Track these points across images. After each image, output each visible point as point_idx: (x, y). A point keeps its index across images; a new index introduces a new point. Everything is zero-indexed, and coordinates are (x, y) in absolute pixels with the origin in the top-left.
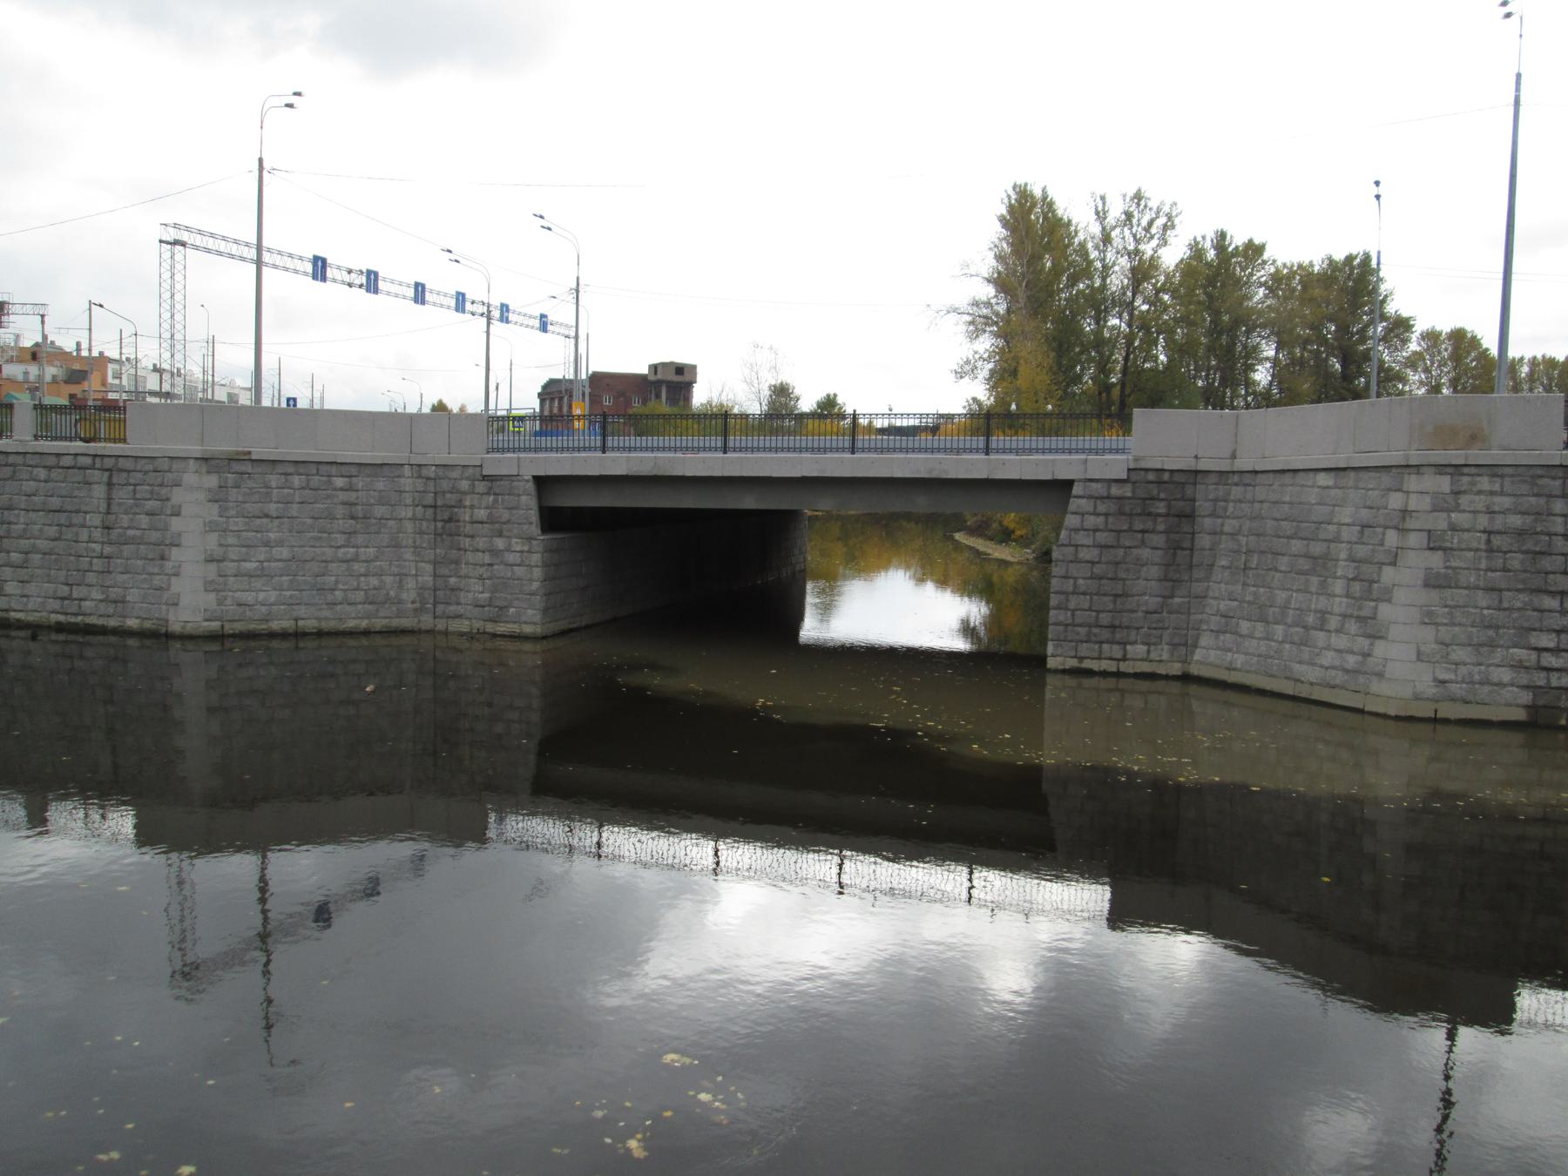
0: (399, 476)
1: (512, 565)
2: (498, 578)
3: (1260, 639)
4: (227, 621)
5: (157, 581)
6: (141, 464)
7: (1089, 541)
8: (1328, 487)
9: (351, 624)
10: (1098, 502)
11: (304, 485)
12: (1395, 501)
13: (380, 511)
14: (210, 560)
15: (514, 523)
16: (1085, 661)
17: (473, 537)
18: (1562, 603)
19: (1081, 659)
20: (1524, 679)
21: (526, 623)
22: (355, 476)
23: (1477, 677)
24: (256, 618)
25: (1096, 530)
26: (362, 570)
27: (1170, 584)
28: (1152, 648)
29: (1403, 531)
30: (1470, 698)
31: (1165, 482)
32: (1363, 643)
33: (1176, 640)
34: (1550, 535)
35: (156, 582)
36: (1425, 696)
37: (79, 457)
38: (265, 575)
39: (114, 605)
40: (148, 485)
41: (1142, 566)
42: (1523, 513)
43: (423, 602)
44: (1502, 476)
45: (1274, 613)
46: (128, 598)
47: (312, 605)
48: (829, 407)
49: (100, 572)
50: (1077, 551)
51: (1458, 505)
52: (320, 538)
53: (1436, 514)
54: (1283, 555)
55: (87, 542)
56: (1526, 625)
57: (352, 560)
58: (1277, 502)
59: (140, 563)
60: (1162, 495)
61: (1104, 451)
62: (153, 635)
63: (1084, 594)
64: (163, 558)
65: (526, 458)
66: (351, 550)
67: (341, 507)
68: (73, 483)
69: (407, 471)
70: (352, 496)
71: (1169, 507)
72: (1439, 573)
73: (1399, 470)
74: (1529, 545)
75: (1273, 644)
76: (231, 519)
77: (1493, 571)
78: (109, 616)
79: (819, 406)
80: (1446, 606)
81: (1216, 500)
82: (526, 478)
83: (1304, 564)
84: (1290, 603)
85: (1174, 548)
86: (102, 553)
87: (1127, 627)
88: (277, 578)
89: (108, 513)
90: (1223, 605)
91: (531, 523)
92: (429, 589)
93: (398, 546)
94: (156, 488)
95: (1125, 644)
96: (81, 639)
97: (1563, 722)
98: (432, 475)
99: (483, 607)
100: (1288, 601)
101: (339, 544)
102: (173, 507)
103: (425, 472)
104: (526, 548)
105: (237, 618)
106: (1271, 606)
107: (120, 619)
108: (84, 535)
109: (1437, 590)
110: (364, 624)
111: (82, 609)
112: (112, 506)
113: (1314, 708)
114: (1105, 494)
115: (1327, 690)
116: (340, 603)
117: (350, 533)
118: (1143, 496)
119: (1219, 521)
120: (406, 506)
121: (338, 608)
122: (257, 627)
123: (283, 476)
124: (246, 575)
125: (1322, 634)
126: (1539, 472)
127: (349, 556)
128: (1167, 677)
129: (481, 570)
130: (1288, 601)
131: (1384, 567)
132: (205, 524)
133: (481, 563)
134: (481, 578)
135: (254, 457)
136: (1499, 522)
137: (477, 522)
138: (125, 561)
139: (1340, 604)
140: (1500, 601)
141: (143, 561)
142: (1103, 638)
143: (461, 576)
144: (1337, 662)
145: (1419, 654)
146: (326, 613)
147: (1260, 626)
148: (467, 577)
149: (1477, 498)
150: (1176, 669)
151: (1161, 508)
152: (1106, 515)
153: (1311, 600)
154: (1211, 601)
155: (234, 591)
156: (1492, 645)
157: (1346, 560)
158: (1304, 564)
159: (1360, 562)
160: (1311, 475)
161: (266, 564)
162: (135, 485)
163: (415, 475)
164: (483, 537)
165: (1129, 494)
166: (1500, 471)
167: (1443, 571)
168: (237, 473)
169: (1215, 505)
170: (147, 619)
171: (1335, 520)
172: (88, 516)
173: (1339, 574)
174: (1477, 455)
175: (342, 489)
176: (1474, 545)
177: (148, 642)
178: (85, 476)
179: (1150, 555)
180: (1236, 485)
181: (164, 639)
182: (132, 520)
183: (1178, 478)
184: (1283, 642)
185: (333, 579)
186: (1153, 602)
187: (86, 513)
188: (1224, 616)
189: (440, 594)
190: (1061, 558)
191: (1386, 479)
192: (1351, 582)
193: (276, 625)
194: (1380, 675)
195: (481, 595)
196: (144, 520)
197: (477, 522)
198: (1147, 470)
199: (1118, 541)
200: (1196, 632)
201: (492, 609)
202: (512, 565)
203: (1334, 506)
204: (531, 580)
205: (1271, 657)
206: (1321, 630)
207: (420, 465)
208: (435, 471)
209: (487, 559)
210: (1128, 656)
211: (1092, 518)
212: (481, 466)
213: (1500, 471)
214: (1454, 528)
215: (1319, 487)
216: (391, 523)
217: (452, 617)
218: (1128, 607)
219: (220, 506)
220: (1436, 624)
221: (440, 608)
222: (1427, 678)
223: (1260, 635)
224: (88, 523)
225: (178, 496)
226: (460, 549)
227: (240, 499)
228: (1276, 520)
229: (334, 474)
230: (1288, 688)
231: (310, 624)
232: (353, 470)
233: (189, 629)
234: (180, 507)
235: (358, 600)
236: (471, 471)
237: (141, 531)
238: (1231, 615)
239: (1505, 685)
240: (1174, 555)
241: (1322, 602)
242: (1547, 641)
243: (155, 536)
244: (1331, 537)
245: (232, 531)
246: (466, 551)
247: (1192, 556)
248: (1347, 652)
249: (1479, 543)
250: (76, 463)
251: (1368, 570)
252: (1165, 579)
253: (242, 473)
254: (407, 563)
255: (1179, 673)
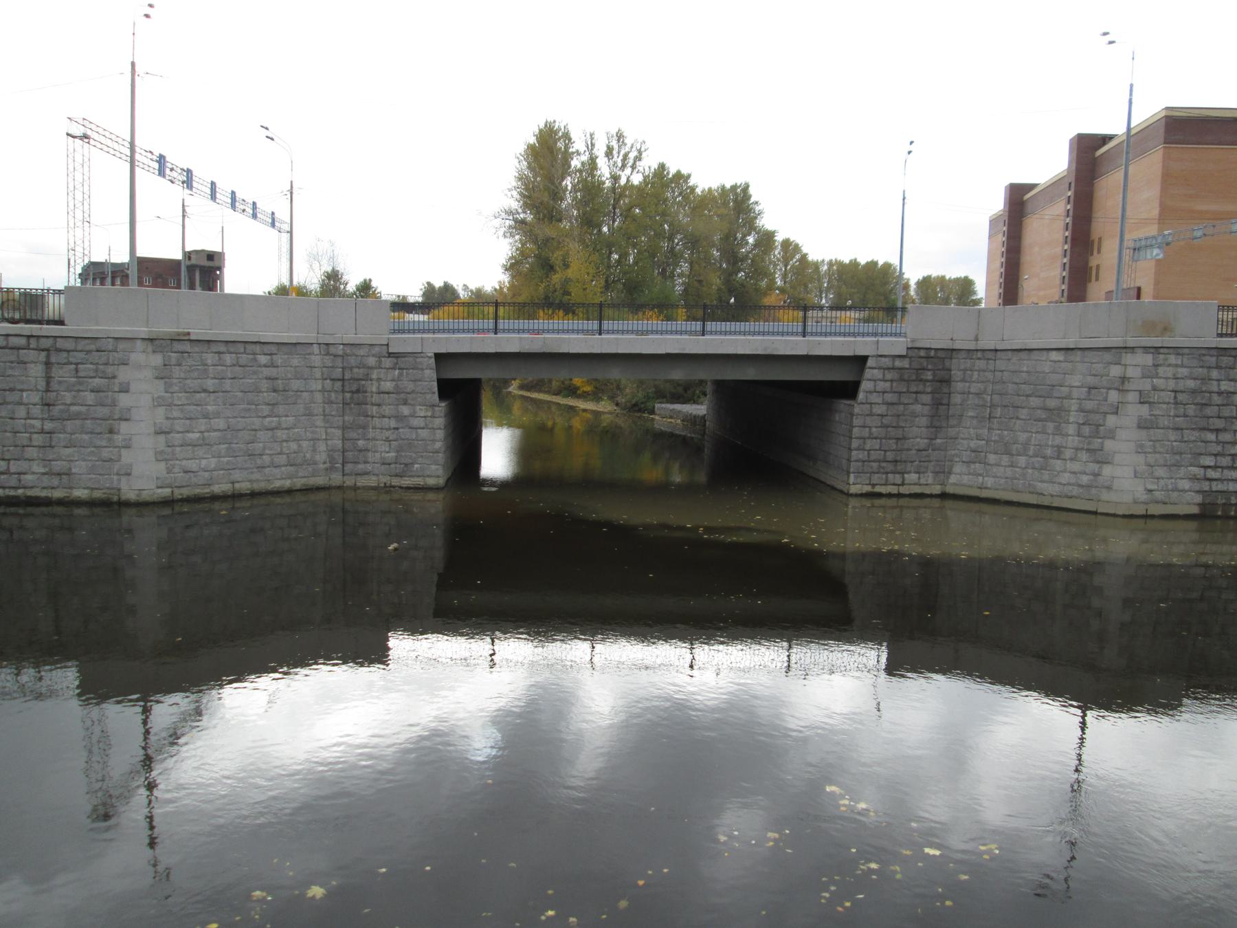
0: (309, 354)
1: (417, 428)
2: (403, 440)
3: (1005, 466)
4: (176, 487)
5: (105, 453)
6: (81, 345)
7: (879, 400)
8: (1059, 361)
9: (277, 484)
10: (886, 372)
11: (235, 362)
12: (1115, 371)
13: (296, 384)
14: (159, 432)
15: (418, 393)
16: (877, 487)
17: (379, 405)
18: (1217, 436)
19: (874, 485)
20: (1197, 486)
21: (428, 476)
22: (275, 354)
23: (1170, 487)
24: (200, 483)
25: (884, 392)
26: (284, 437)
27: (934, 429)
28: (922, 475)
29: (1122, 391)
30: (1167, 500)
31: (932, 357)
32: (1094, 467)
33: (937, 469)
34: (1211, 393)
35: (106, 455)
36: (1140, 500)
37: (10, 338)
38: (206, 444)
39: (58, 477)
40: (91, 363)
41: (916, 417)
42: (1195, 379)
43: (332, 460)
44: (1182, 355)
45: (1017, 449)
46: (74, 470)
47: (246, 469)
48: (365, 288)
49: (40, 447)
50: (871, 407)
51: (1157, 373)
52: (249, 409)
53: (1144, 379)
54: (1023, 408)
55: (25, 419)
56: (1198, 451)
57: (277, 428)
58: (1016, 372)
59: (86, 437)
60: (930, 367)
61: (647, 332)
62: (105, 504)
63: (876, 438)
64: (111, 431)
65: (428, 338)
66: (275, 419)
67: (265, 381)
68: (5, 362)
69: (316, 349)
70: (272, 372)
71: (934, 375)
72: (1146, 419)
73: (1118, 350)
74: (1199, 400)
75: (1017, 469)
76: (175, 395)
77: (1178, 417)
78: (53, 488)
79: (358, 289)
80: (1150, 441)
81: (965, 370)
82: (430, 355)
83: (1041, 414)
84: (1030, 441)
85: (937, 404)
86: (43, 429)
87: (905, 462)
88: (216, 446)
89: (47, 391)
90: (973, 444)
91: (434, 393)
92: (339, 450)
93: (310, 415)
94: (101, 367)
95: (903, 473)
96: (21, 511)
97: (1233, 513)
98: (341, 353)
99: (390, 464)
100: (1029, 439)
101: (265, 415)
102: (120, 384)
103: (332, 350)
104: (429, 414)
105: (185, 484)
106: (1014, 444)
107: (65, 490)
108: (21, 412)
109: (1145, 430)
110: (287, 484)
111: (23, 482)
112: (52, 384)
113: (1070, 514)
114: (891, 366)
115: (1065, 499)
116: (268, 467)
117: (273, 404)
118: (916, 367)
119: (967, 384)
120: (316, 379)
121: (267, 471)
122: (202, 491)
123: (217, 355)
124: (189, 445)
125: (1059, 462)
126: (1203, 352)
127: (274, 425)
128: (931, 496)
129: (388, 433)
130: (1029, 439)
131: (1108, 416)
132: (153, 400)
133: (387, 427)
134: (387, 440)
135: (193, 337)
136: (1181, 385)
137: (382, 393)
138: (68, 435)
139: (1073, 441)
140: (1182, 437)
141: (89, 435)
142: (889, 470)
143: (368, 439)
144: (1072, 481)
145: (1135, 472)
146: (256, 476)
147: (1005, 460)
148: (374, 439)
149: (1168, 369)
150: (937, 490)
151: (929, 375)
152: (892, 381)
153: (1048, 439)
154: (962, 441)
155: (180, 460)
156: (1177, 465)
157: (1077, 411)
158: (1041, 414)
159: (1089, 412)
160: (1045, 352)
161: (206, 434)
162: (77, 364)
163: (322, 353)
164: (390, 405)
165: (907, 366)
166: (1180, 351)
167: (1148, 417)
168: (179, 352)
169: (964, 373)
170: (97, 489)
171: (1066, 384)
172: (25, 394)
173: (1071, 421)
174: (1168, 341)
175: (265, 366)
176: (1167, 400)
177: (97, 510)
178: (18, 356)
179: (922, 410)
180: (979, 359)
181: (116, 507)
182: (75, 396)
183: (941, 354)
184: (1026, 468)
185: (261, 445)
186: (923, 443)
187: (22, 391)
188: (974, 451)
189: (349, 455)
190: (861, 413)
191: (1107, 356)
192: (1082, 426)
193: (217, 489)
194: (1109, 488)
195: (387, 455)
196: (90, 398)
197: (382, 393)
198: (919, 349)
199: (900, 399)
200: (950, 463)
201: (398, 466)
202: (417, 428)
203: (1065, 374)
204: (434, 441)
205: (1016, 479)
206: (1058, 459)
207: (327, 344)
208: (343, 349)
209: (393, 423)
210: (906, 482)
211: (882, 383)
212: (388, 345)
213: (1180, 351)
214: (1155, 389)
215: (1051, 361)
216: (305, 394)
217: (359, 474)
218: (906, 446)
219: (166, 383)
220: (1145, 453)
221: (349, 467)
222: (1141, 489)
223: (1007, 464)
224: (25, 400)
225: (124, 374)
226: (367, 416)
227: (182, 375)
228: (1016, 383)
229: (258, 352)
230: (1033, 500)
231: (244, 487)
232: (273, 349)
233: (146, 496)
234: (128, 383)
235: (282, 463)
236: (377, 349)
237: (87, 408)
238: (980, 450)
239: (1186, 491)
240: (937, 409)
241: (1058, 440)
242: (1209, 461)
243: (103, 411)
244: (1064, 395)
245: (175, 405)
246: (373, 417)
247: (948, 409)
248: (1080, 473)
249: (1170, 398)
250: (8, 344)
251: (1096, 418)
252: (931, 426)
253: (182, 353)
254: (318, 429)
255: (939, 492)
